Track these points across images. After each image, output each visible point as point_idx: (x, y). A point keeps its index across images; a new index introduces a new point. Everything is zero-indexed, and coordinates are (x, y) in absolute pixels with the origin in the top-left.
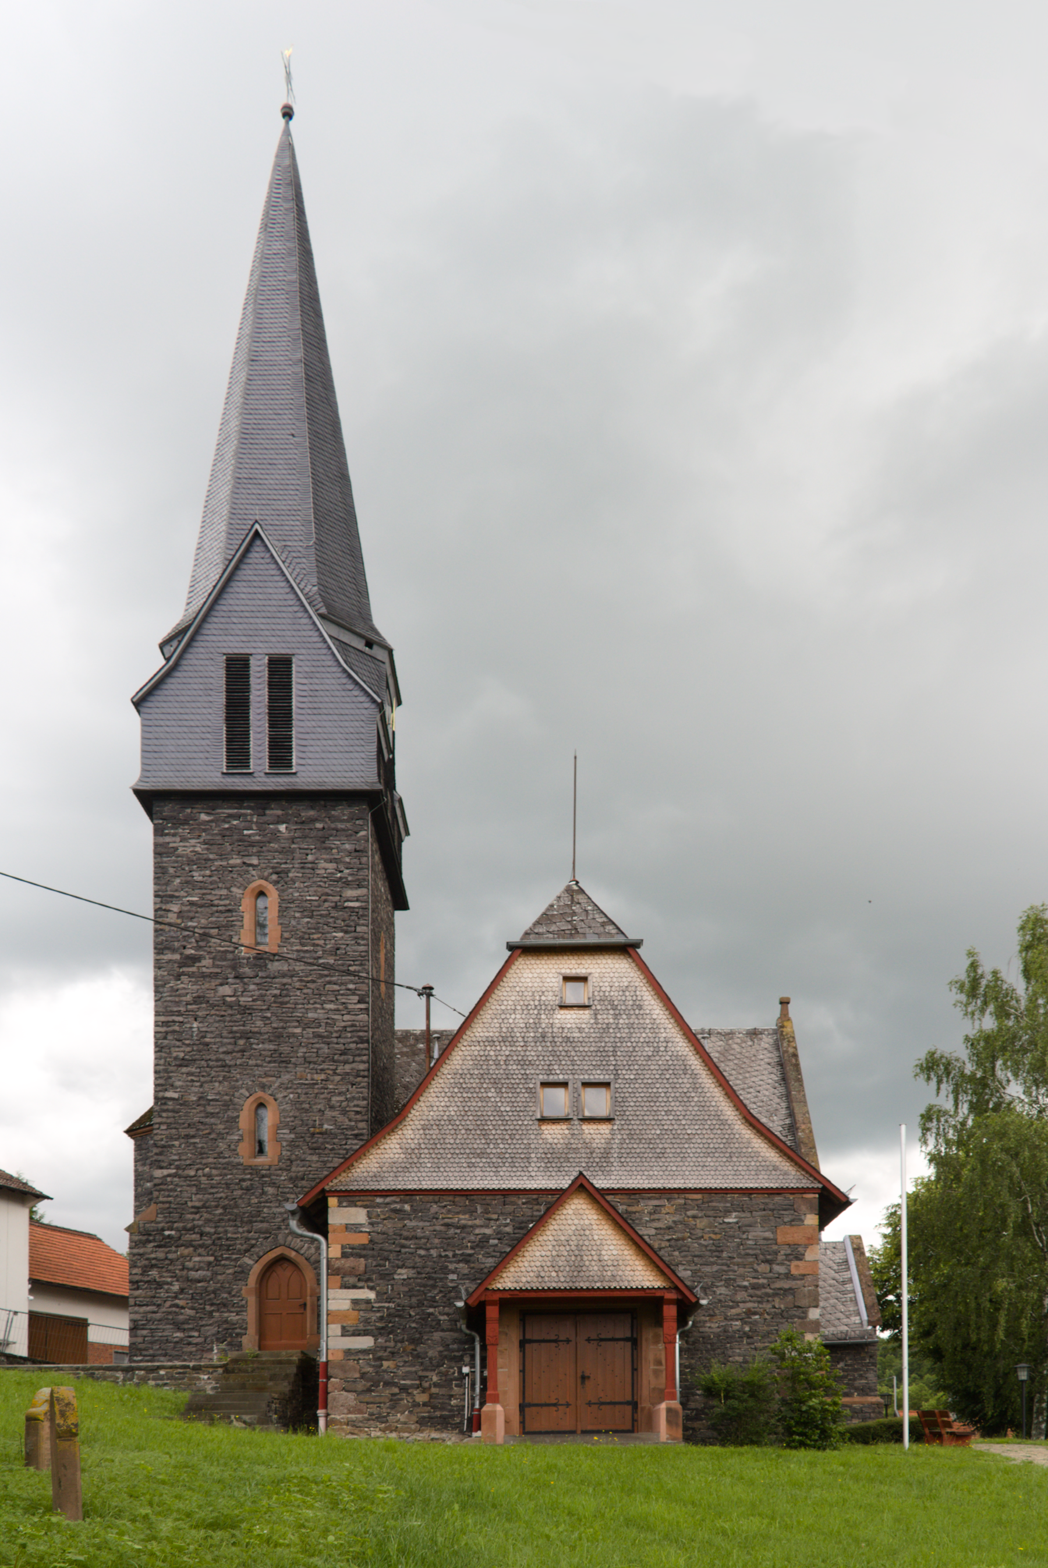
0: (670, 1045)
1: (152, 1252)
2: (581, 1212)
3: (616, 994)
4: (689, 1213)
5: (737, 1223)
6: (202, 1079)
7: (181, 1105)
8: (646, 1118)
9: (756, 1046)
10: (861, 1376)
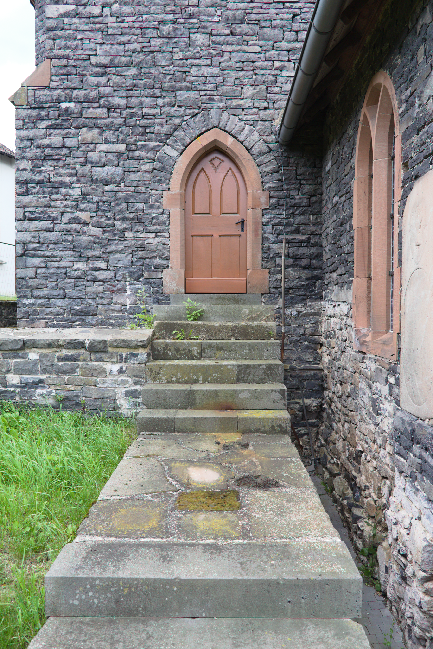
1: (46, 135)
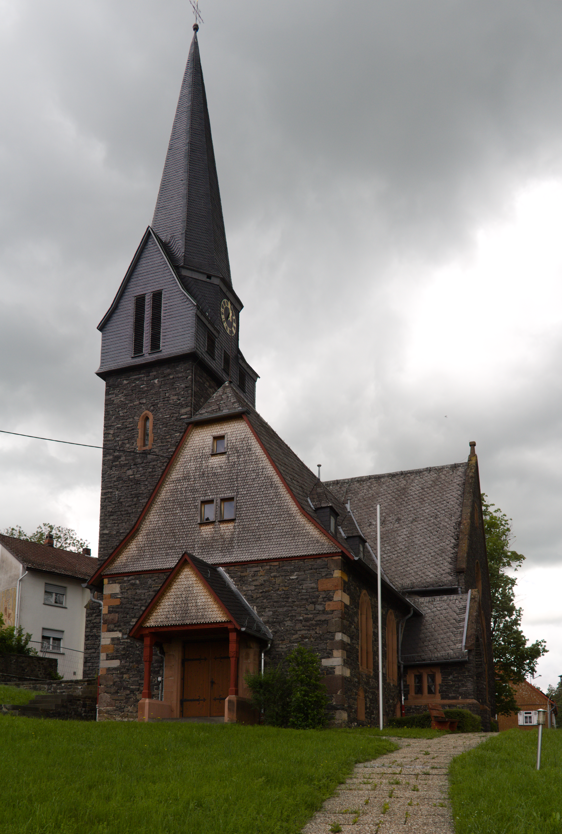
0: (264, 470)
1: (95, 619)
2: (188, 576)
3: (238, 443)
4: (272, 575)
5: (297, 579)
6: (119, 522)
7: (110, 537)
8: (251, 517)
9: (454, 475)
10: (463, 685)
